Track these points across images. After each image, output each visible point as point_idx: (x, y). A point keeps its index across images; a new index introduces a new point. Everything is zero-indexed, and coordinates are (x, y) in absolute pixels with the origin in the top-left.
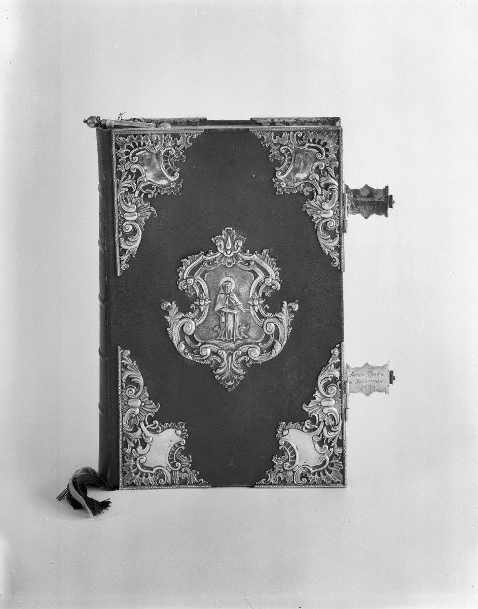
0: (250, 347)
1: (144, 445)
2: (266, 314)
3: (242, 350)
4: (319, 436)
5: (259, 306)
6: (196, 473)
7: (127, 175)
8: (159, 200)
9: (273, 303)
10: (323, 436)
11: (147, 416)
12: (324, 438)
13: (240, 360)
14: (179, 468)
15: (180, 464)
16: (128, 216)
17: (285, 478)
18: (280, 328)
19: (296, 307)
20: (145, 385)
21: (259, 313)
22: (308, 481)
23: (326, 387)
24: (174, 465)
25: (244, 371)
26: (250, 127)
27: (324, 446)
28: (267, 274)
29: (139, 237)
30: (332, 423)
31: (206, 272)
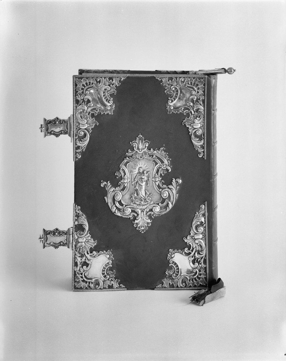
0: (154, 206)
1: (87, 265)
2: (163, 186)
3: (149, 208)
4: (89, 107)
5: (158, 181)
6: (162, 84)
7: (200, 261)
8: (182, 247)
9: (167, 180)
10: (195, 257)
11: (190, 118)
12: (196, 259)
13: (148, 214)
14: (108, 279)
15: (109, 276)
16: (81, 126)
17: (173, 283)
18: (171, 195)
19: (180, 181)
20: (89, 230)
21: (159, 186)
22: (186, 285)
23: (197, 228)
24: (105, 277)
25: (151, 220)
26: (155, 75)
27: (195, 264)
28: (162, 162)
29: (195, 223)
30: (200, 249)
31: (127, 162)
